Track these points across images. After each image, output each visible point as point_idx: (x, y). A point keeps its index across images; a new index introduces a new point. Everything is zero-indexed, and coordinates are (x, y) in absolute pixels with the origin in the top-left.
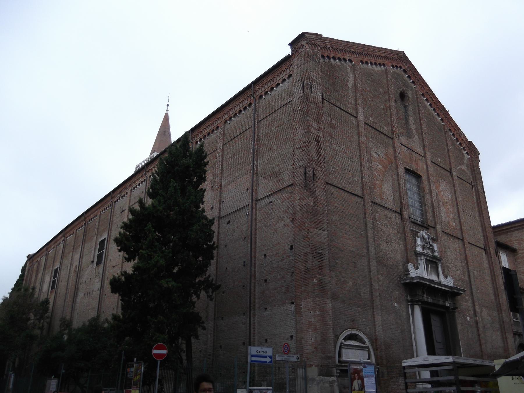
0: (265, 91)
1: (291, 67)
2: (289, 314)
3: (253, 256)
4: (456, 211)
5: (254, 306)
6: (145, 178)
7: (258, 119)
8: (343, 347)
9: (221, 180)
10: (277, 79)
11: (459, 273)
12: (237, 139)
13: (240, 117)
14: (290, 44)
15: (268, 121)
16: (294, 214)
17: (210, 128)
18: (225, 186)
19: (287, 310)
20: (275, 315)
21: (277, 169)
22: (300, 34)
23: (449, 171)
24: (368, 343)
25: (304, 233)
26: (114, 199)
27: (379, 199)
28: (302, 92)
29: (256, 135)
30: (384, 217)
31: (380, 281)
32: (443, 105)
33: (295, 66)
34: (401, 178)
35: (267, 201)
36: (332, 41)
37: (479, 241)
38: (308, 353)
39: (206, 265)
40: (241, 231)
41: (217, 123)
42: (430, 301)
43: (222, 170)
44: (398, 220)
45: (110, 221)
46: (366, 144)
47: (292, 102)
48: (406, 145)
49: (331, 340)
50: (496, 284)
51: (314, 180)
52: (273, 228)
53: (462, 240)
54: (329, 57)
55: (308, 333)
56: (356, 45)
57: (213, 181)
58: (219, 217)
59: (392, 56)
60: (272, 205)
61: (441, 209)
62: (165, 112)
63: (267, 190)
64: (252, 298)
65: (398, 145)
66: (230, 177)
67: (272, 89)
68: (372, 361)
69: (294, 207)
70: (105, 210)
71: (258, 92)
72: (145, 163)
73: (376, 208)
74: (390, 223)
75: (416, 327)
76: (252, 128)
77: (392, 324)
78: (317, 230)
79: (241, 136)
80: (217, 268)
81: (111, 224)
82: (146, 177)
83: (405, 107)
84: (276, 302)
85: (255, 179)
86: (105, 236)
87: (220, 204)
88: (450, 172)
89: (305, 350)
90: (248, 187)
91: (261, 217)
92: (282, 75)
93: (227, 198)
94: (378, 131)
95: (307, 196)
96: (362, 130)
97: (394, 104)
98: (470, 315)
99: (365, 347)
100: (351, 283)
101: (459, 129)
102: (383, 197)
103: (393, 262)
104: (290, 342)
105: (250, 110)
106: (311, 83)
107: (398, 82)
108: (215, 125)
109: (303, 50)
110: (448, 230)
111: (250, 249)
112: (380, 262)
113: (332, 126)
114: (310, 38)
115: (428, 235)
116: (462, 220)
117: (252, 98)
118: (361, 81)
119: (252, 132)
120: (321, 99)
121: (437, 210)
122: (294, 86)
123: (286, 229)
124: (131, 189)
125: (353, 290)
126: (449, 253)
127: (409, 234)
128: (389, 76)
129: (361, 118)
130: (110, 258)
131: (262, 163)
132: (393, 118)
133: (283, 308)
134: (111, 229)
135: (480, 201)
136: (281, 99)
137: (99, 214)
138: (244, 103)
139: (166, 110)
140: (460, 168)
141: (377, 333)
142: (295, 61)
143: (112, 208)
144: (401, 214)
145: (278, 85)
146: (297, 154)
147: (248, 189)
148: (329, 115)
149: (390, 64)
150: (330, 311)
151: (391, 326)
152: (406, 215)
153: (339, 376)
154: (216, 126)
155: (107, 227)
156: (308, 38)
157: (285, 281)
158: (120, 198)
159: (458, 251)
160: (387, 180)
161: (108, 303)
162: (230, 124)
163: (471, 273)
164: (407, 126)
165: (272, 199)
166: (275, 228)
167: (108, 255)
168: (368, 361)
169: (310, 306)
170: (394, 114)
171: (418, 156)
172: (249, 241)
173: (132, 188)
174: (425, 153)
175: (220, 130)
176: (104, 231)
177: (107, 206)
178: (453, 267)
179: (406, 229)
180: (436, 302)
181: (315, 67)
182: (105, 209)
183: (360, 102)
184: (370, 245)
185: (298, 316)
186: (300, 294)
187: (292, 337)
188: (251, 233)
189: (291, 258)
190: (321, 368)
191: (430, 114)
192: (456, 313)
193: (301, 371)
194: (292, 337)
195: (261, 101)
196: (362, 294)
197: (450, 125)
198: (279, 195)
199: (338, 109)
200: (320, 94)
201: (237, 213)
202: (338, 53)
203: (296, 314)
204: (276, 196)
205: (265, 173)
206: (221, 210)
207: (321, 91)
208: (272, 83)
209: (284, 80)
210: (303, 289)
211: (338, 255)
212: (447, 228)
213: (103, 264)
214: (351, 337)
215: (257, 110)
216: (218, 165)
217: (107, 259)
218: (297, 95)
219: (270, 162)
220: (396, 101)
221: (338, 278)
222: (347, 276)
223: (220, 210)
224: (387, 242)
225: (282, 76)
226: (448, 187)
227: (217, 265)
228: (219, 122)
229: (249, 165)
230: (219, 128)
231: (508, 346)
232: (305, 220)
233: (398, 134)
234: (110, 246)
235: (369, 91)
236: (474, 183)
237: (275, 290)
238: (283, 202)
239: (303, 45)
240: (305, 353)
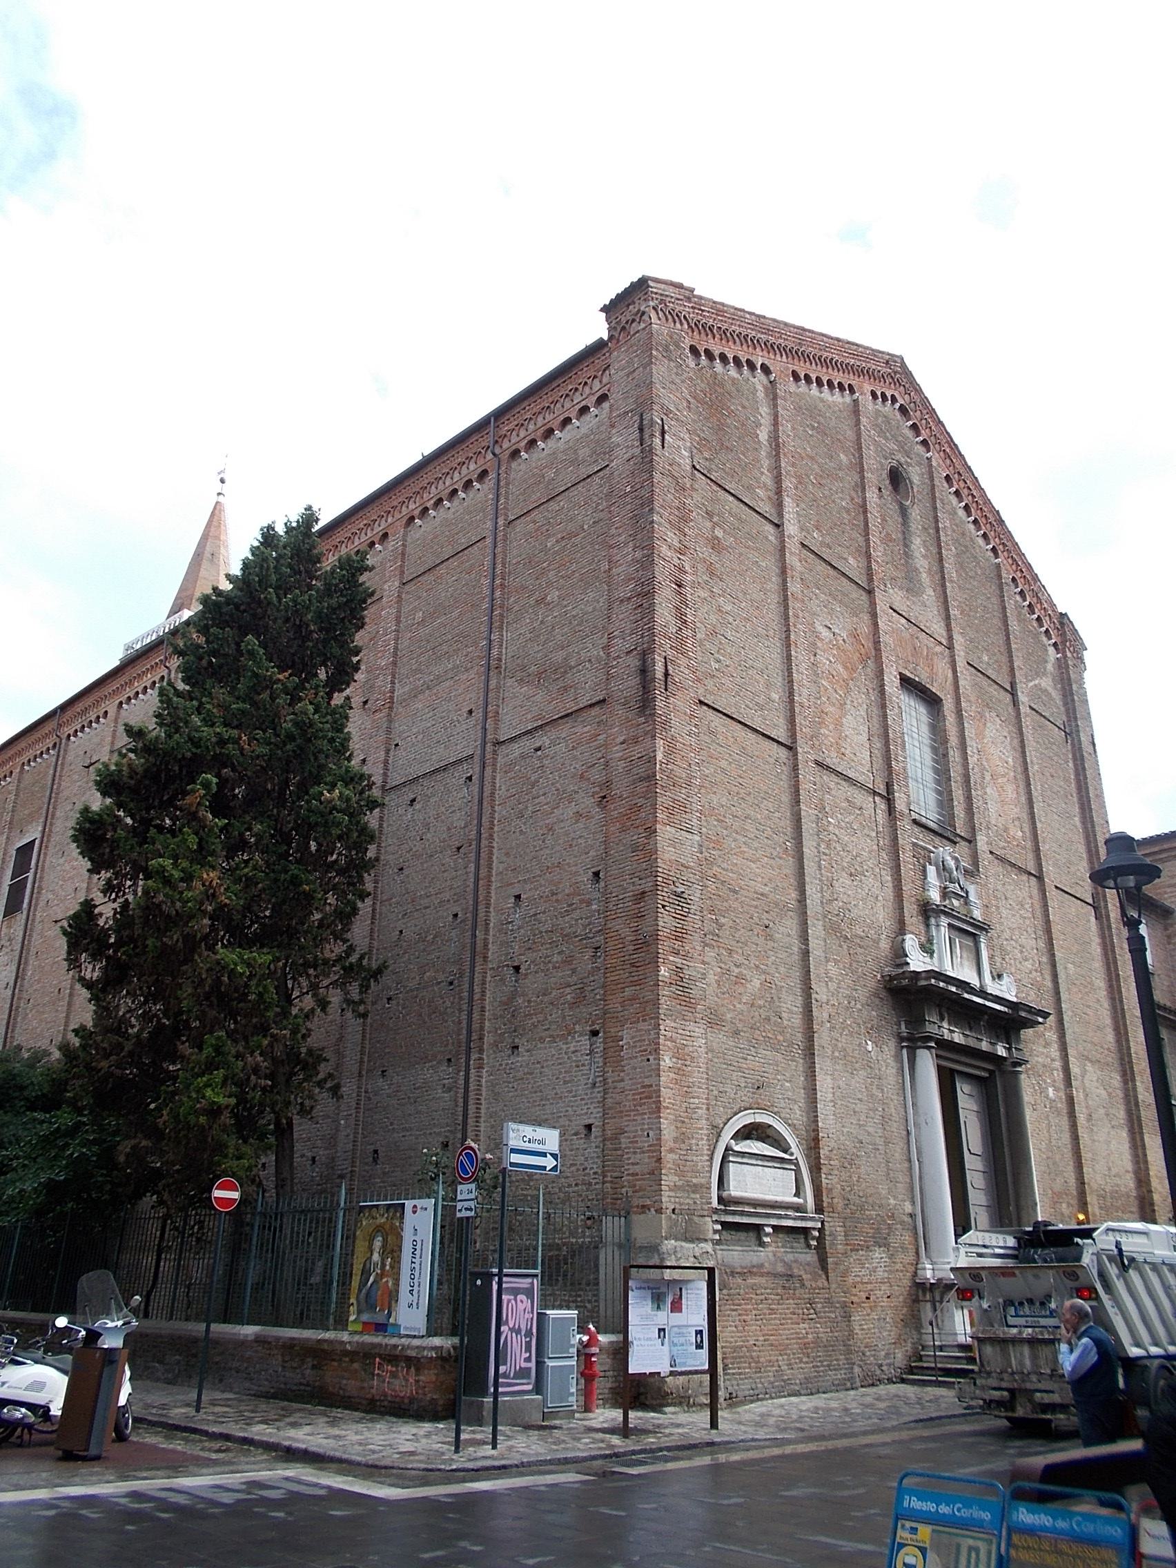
0: (529, 438)
1: (607, 372)
2: (583, 1065)
3: (481, 898)
4: (1023, 799)
5: (481, 1038)
6: (165, 673)
7: (506, 515)
8: (731, 1159)
9: (393, 682)
10: (563, 406)
11: (1030, 966)
12: (442, 570)
13: (452, 510)
14: (605, 309)
15: (534, 522)
16: (608, 784)
17: (363, 538)
18: (405, 700)
19: (579, 1054)
20: (543, 1067)
21: (559, 656)
22: (635, 280)
23: (1009, 689)
24: (797, 1152)
25: (635, 837)
26: (66, 729)
27: (834, 754)
28: (637, 443)
29: (499, 560)
30: (844, 805)
31: (831, 979)
32: (998, 512)
33: (617, 370)
34: (890, 701)
35: (528, 744)
36: (719, 309)
37: (1081, 883)
38: (637, 1174)
39: (347, 915)
40: (449, 829)
41: (383, 525)
42: (956, 1040)
43: (395, 655)
44: (882, 816)
45: (51, 793)
46: (803, 601)
47: (607, 471)
48: (904, 614)
49: (702, 1139)
50: (1121, 1001)
51: (666, 690)
52: (541, 824)
53: (1040, 878)
54: (709, 354)
55: (639, 1118)
56: (782, 326)
57: (370, 686)
58: (383, 786)
59: (874, 367)
60: (539, 758)
61: (988, 790)
62: (215, 499)
63: (529, 716)
64: (476, 1016)
65: (883, 611)
66: (420, 675)
67: (549, 433)
68: (806, 1201)
69: (607, 764)
70: (35, 761)
71: (506, 440)
72: (154, 638)
73: (825, 777)
74: (861, 823)
75: (921, 1111)
76: (489, 541)
77: (860, 1100)
78: (673, 830)
79: (454, 563)
80: (372, 930)
81: (52, 800)
82: (167, 671)
83: (904, 512)
84: (545, 1030)
85: (493, 683)
86: (33, 833)
87: (388, 751)
88: (1013, 693)
89: (628, 1164)
90: (473, 706)
91: (508, 790)
92: (577, 394)
93: (408, 734)
94: (835, 568)
95: (646, 734)
96: (792, 560)
97: (876, 499)
98: (1055, 1081)
99: (789, 1161)
100: (757, 983)
101: (1036, 578)
102: (843, 750)
103: (866, 929)
104: (583, 1141)
105: (483, 490)
106: (662, 420)
107: (886, 439)
108: (377, 529)
109: (642, 325)
110: (1004, 848)
111: (472, 880)
112: (833, 929)
113: (715, 545)
114: (661, 295)
115: (956, 859)
116: (1039, 825)
117: (490, 456)
118: (794, 429)
119: (489, 551)
120: (688, 468)
121: (979, 793)
122: (613, 426)
123: (581, 825)
124: (117, 702)
125: (761, 1002)
126: (1004, 912)
127: (906, 856)
128: (864, 420)
129: (791, 528)
130: (46, 895)
131: (511, 642)
132: (873, 535)
133: (564, 1047)
134: (53, 816)
135: (1086, 778)
136: (575, 462)
137: (18, 770)
138: (464, 471)
139: (219, 494)
140: (1035, 685)
141: (820, 1124)
142: (619, 359)
143: (58, 756)
144: (889, 800)
145: (567, 421)
146: (621, 617)
147: (470, 712)
148: (707, 513)
149: (868, 388)
150: (700, 1057)
151: (856, 1104)
152: (900, 805)
153: (718, 1242)
154: (381, 534)
155: (41, 808)
156: (656, 293)
157: (574, 971)
158: (83, 727)
159: (1027, 906)
160: (856, 704)
161: (35, 1023)
162: (423, 529)
163: (1060, 968)
164: (907, 562)
165: (542, 739)
166: (547, 822)
167: (40, 888)
168: (796, 1200)
169: (647, 1042)
170: (874, 526)
171: (932, 645)
172: (472, 856)
173: (124, 699)
174: (950, 638)
175: (391, 543)
176: (31, 818)
177: (44, 749)
178: (1016, 951)
179: (901, 841)
180: (972, 1043)
181: (674, 376)
182: (35, 757)
183: (788, 483)
184: (807, 879)
185: (610, 1069)
186: (620, 1009)
187: (589, 1127)
188: (479, 833)
189: (594, 907)
190: (674, 1216)
191: (963, 534)
192: (1023, 1076)
193: (610, 1225)
194: (589, 1127)
195: (514, 465)
196: (784, 1015)
197: (1014, 567)
198: (564, 730)
199: (731, 499)
200: (687, 454)
201: (439, 777)
202: (735, 343)
203: (605, 1064)
204: (553, 733)
205: (523, 668)
206: (390, 767)
207: (689, 444)
208: (549, 417)
209: (584, 410)
210: (628, 992)
211: (725, 904)
212: (1002, 844)
213: (25, 913)
214: (750, 1132)
215: (503, 491)
216: (385, 641)
217: (37, 899)
218: (624, 451)
219: (538, 636)
220: (880, 489)
221: (723, 966)
222: (746, 962)
223: (386, 768)
224: (851, 875)
225: (577, 398)
226: (1006, 734)
227: (372, 923)
228: (390, 520)
229: (475, 644)
230: (391, 538)
231: (1147, 1169)
232: (641, 801)
233: (883, 579)
234: (47, 862)
235: (812, 458)
236: (1070, 726)
237: (544, 995)
238: (574, 748)
239: (644, 313)
240: (628, 1175)
